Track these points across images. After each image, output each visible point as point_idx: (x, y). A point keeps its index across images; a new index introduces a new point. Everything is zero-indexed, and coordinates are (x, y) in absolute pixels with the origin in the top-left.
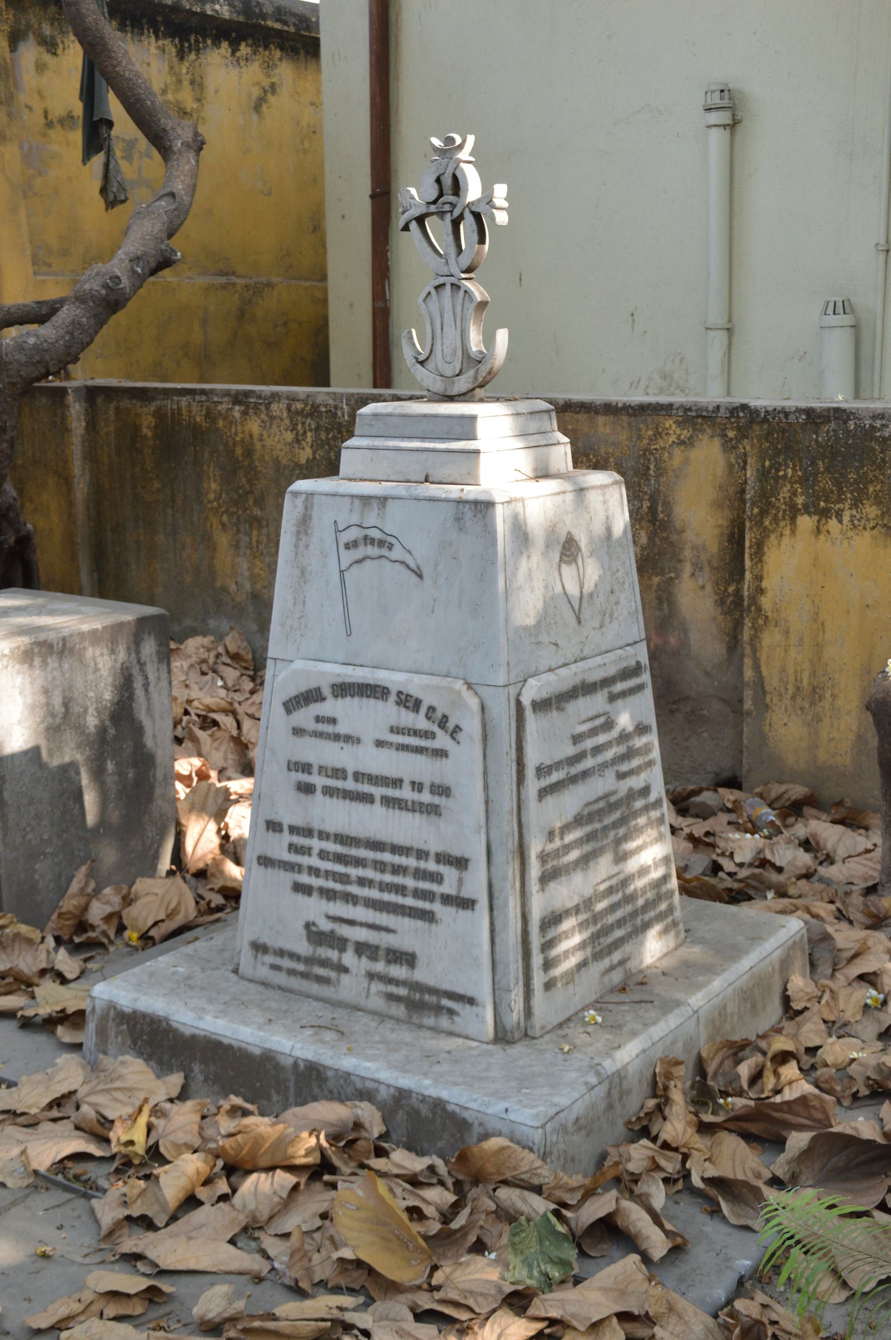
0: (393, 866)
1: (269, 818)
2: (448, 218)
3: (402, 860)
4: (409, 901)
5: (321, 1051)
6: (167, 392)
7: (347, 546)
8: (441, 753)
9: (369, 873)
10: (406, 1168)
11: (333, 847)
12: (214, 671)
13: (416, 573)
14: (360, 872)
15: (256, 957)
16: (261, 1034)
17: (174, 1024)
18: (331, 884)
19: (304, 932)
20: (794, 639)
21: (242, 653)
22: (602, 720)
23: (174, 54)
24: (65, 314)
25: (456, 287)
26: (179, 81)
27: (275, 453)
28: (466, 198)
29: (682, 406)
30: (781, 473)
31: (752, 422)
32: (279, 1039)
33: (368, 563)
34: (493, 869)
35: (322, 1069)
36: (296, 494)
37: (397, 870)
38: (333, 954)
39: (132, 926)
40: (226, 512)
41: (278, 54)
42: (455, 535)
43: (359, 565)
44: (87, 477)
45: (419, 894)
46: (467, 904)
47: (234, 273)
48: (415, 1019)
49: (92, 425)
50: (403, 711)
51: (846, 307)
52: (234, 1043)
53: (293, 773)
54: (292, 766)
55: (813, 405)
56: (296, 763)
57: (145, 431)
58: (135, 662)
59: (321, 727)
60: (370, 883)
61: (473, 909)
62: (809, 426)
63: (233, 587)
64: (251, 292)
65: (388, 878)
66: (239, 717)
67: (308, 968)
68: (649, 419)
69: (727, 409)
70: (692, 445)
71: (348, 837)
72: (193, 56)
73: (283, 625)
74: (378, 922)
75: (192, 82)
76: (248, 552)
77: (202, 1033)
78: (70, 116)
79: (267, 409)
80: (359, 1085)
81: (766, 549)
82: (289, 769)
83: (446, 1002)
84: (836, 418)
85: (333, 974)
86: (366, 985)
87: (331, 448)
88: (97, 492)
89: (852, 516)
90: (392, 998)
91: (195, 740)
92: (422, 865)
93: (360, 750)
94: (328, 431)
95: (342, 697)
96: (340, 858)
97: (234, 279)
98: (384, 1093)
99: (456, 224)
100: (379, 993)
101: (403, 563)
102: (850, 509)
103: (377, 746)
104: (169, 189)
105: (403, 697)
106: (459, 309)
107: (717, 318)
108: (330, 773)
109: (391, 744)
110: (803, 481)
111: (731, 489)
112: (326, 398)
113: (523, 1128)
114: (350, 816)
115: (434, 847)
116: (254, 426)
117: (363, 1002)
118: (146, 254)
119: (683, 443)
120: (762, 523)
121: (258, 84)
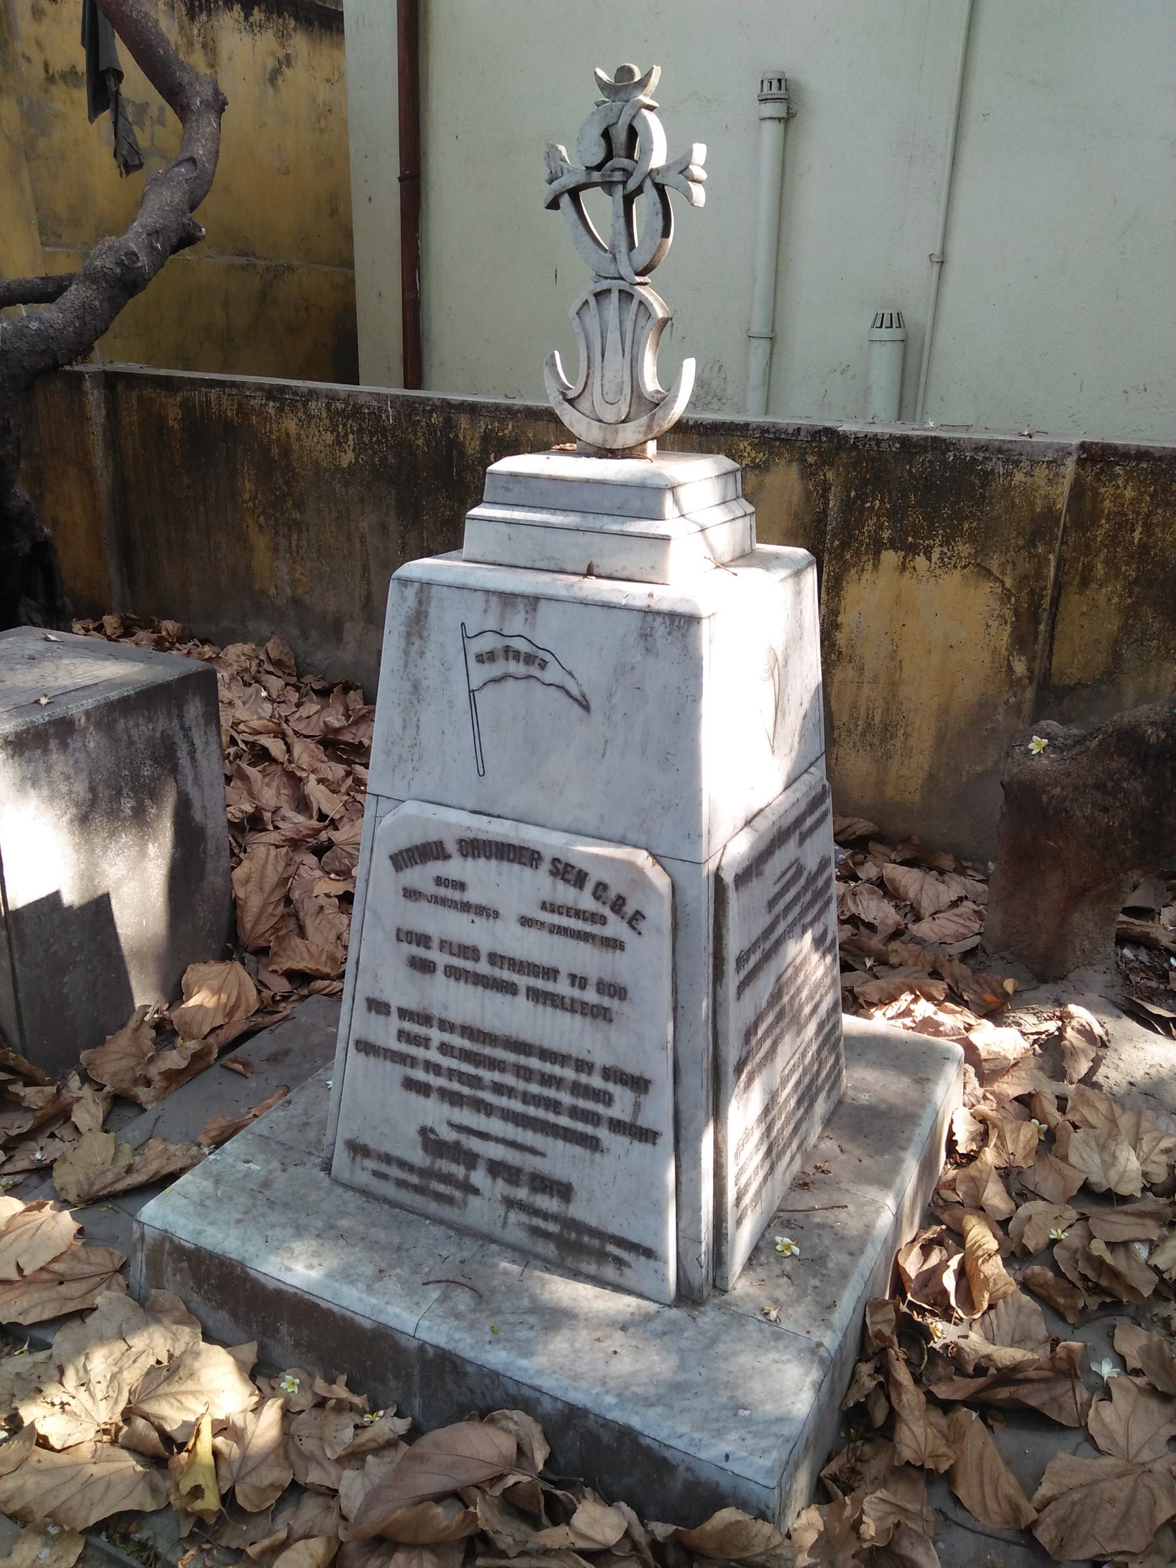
0: (543, 1075)
1: (371, 996)
2: (619, 191)
3: (557, 1070)
4: (564, 1121)
5: (457, 1336)
6: (193, 382)
7: (480, 658)
8: (615, 944)
9: (509, 1080)
10: (594, 1540)
11: (457, 1041)
12: (257, 682)
13: (580, 703)
14: (497, 1076)
15: (354, 1159)
16: (373, 1301)
17: (252, 1272)
18: (455, 1086)
19: (419, 1139)
20: (868, 675)
21: (285, 659)
22: (794, 869)
23: (184, 12)
24: (74, 295)
25: (626, 296)
26: (190, 44)
27: (315, 454)
28: (648, 162)
29: (758, 427)
30: (868, 505)
31: (839, 448)
32: (398, 1310)
33: (510, 683)
34: (681, 1091)
35: (458, 1362)
36: (405, 582)
37: (548, 1080)
38: (459, 1171)
39: (185, 1032)
40: (264, 513)
41: (292, 23)
42: (639, 657)
43: (497, 685)
44: (111, 469)
45: (574, 1113)
46: (648, 1136)
47: (254, 254)
48: (569, 1262)
49: (113, 413)
50: (560, 884)
51: (896, 320)
52: (336, 1309)
53: (405, 945)
54: (402, 936)
55: (909, 433)
56: (408, 933)
57: (171, 423)
58: (178, 728)
59: (442, 892)
60: (510, 1092)
61: (654, 1143)
62: (902, 455)
63: (273, 591)
64: (272, 274)
65: (535, 1088)
66: (289, 741)
67: (424, 1182)
68: (722, 439)
69: (808, 431)
70: (767, 469)
71: (479, 1031)
72: (204, 17)
73: (388, 753)
74: (520, 1140)
75: (204, 46)
76: (288, 555)
77: (291, 1290)
78: (73, 71)
79: (305, 406)
80: (513, 1390)
81: (844, 584)
82: (399, 939)
83: (611, 1248)
84: (933, 449)
85: (457, 1194)
86: (503, 1213)
87: (375, 453)
88: (121, 484)
89: (942, 553)
90: (536, 1232)
91: (245, 778)
92: (584, 1078)
93: (498, 926)
94: (371, 434)
95: (474, 857)
96: (467, 1056)
97: (254, 260)
98: (547, 1405)
99: (628, 201)
100: (520, 1224)
101: (560, 687)
102: (941, 546)
103: (522, 924)
104: (188, 154)
105: (561, 867)
106: (629, 326)
107: (759, 326)
108: (455, 951)
109: (543, 924)
110: (891, 514)
111: (807, 518)
112: (368, 399)
113: (753, 1486)
114: (483, 1006)
115: (600, 1058)
116: (291, 425)
117: (497, 1232)
118: (165, 227)
119: (757, 466)
120: (842, 555)
121: (273, 54)
